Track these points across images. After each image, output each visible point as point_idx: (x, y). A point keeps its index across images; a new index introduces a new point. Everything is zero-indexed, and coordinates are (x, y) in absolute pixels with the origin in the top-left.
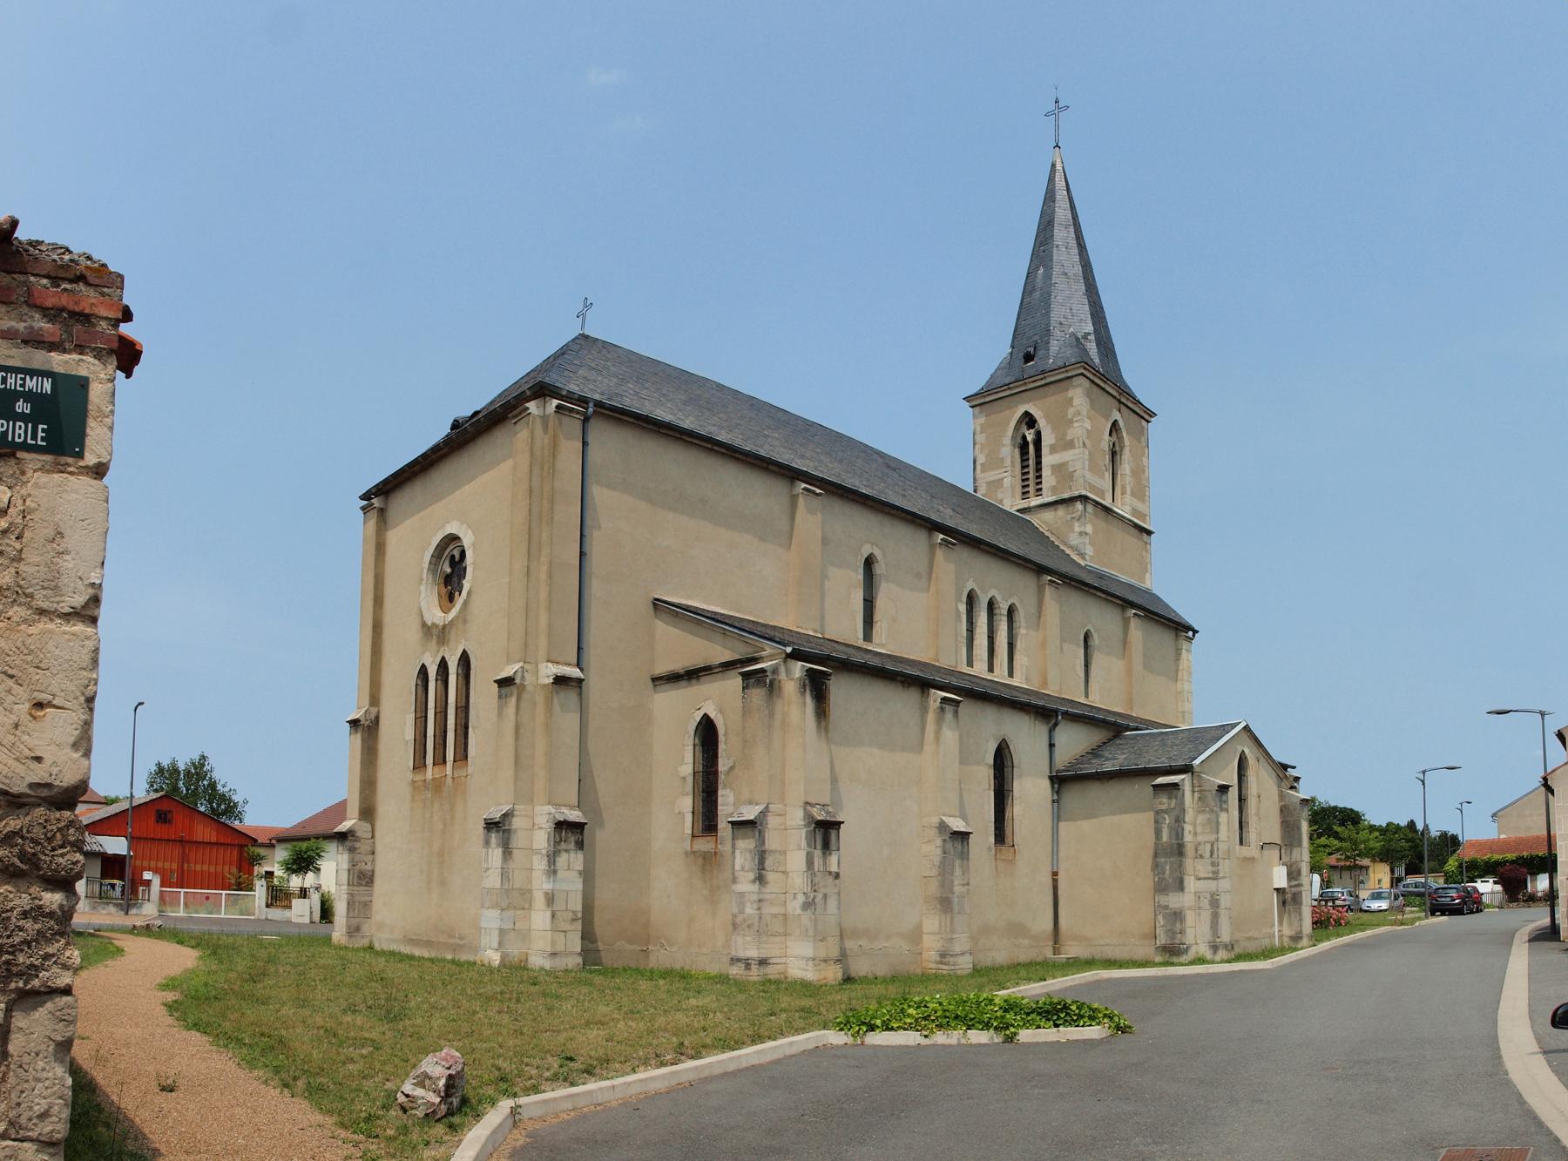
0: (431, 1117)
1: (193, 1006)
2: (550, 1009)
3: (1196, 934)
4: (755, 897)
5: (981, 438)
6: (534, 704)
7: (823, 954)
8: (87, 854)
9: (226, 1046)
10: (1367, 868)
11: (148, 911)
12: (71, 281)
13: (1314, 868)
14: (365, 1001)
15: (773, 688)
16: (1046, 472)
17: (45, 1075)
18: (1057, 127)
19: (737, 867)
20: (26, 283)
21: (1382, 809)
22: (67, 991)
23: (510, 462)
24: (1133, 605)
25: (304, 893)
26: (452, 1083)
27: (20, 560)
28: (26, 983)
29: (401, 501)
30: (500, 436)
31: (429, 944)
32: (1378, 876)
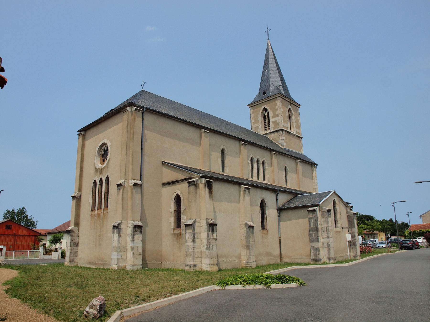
2: (132, 282)
3: (323, 255)
4: (192, 246)
5: (252, 115)
6: (128, 191)
7: (212, 263)
9: (26, 302)
13: (360, 235)
14: (74, 283)
15: (197, 186)
16: (271, 123)
18: (268, 35)
19: (187, 238)
21: (380, 215)
23: (121, 124)
24: (298, 158)
25: (56, 250)
29: (89, 133)
30: (119, 116)
31: (95, 264)
32: (381, 237)
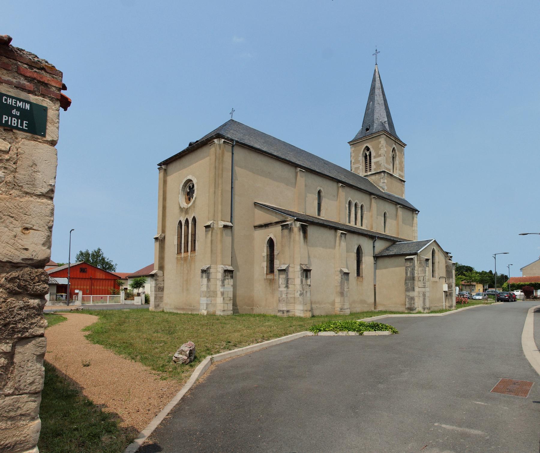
0: (184, 363)
1: (96, 336)
2: (223, 328)
3: (418, 304)
4: (285, 292)
7: (306, 309)
8: (50, 285)
9: (110, 348)
10: (475, 285)
11: (77, 303)
12: (38, 69)
14: (161, 328)
16: (372, 164)
17: (32, 368)
18: (376, 58)
20: (16, 64)
22: (42, 335)
23: (208, 158)
25: (139, 295)
26: (191, 352)
27: (16, 172)
28: (22, 335)
30: (205, 149)
31: (183, 309)
32: (479, 288)
